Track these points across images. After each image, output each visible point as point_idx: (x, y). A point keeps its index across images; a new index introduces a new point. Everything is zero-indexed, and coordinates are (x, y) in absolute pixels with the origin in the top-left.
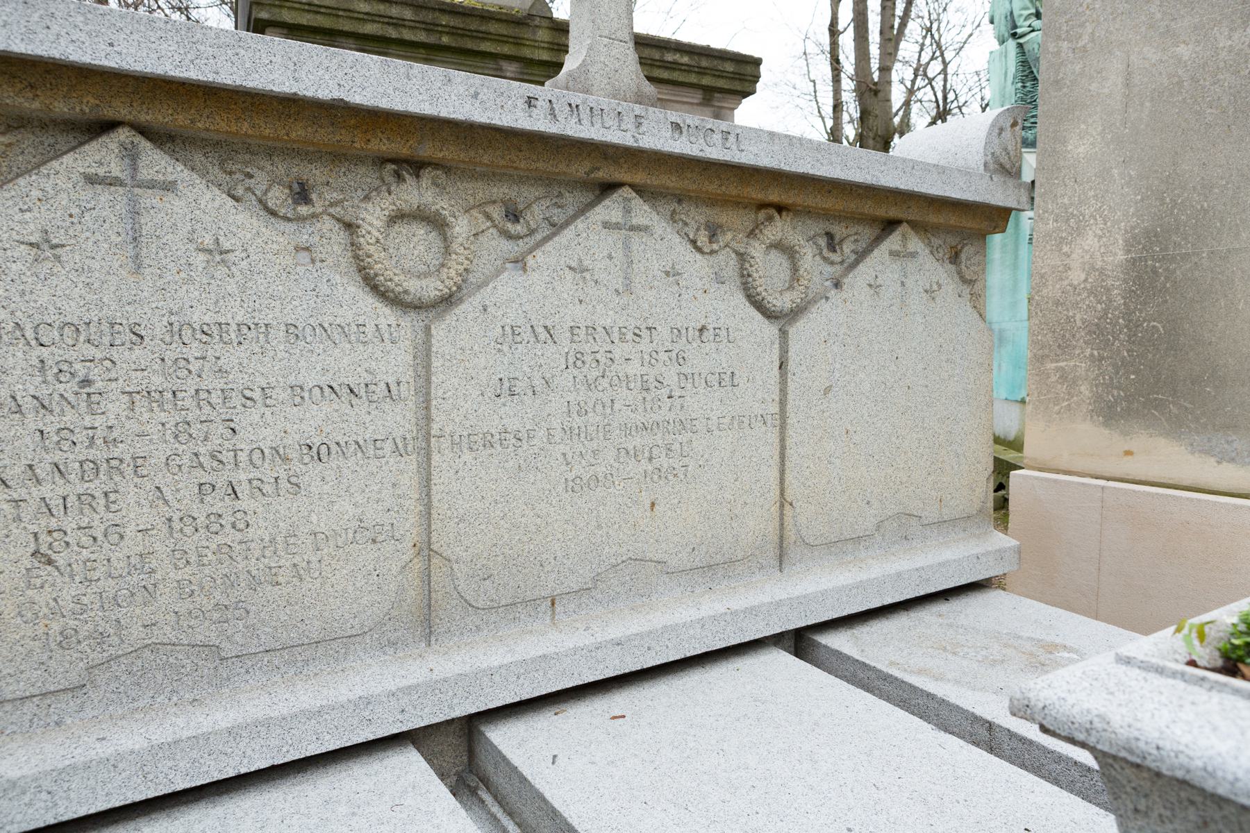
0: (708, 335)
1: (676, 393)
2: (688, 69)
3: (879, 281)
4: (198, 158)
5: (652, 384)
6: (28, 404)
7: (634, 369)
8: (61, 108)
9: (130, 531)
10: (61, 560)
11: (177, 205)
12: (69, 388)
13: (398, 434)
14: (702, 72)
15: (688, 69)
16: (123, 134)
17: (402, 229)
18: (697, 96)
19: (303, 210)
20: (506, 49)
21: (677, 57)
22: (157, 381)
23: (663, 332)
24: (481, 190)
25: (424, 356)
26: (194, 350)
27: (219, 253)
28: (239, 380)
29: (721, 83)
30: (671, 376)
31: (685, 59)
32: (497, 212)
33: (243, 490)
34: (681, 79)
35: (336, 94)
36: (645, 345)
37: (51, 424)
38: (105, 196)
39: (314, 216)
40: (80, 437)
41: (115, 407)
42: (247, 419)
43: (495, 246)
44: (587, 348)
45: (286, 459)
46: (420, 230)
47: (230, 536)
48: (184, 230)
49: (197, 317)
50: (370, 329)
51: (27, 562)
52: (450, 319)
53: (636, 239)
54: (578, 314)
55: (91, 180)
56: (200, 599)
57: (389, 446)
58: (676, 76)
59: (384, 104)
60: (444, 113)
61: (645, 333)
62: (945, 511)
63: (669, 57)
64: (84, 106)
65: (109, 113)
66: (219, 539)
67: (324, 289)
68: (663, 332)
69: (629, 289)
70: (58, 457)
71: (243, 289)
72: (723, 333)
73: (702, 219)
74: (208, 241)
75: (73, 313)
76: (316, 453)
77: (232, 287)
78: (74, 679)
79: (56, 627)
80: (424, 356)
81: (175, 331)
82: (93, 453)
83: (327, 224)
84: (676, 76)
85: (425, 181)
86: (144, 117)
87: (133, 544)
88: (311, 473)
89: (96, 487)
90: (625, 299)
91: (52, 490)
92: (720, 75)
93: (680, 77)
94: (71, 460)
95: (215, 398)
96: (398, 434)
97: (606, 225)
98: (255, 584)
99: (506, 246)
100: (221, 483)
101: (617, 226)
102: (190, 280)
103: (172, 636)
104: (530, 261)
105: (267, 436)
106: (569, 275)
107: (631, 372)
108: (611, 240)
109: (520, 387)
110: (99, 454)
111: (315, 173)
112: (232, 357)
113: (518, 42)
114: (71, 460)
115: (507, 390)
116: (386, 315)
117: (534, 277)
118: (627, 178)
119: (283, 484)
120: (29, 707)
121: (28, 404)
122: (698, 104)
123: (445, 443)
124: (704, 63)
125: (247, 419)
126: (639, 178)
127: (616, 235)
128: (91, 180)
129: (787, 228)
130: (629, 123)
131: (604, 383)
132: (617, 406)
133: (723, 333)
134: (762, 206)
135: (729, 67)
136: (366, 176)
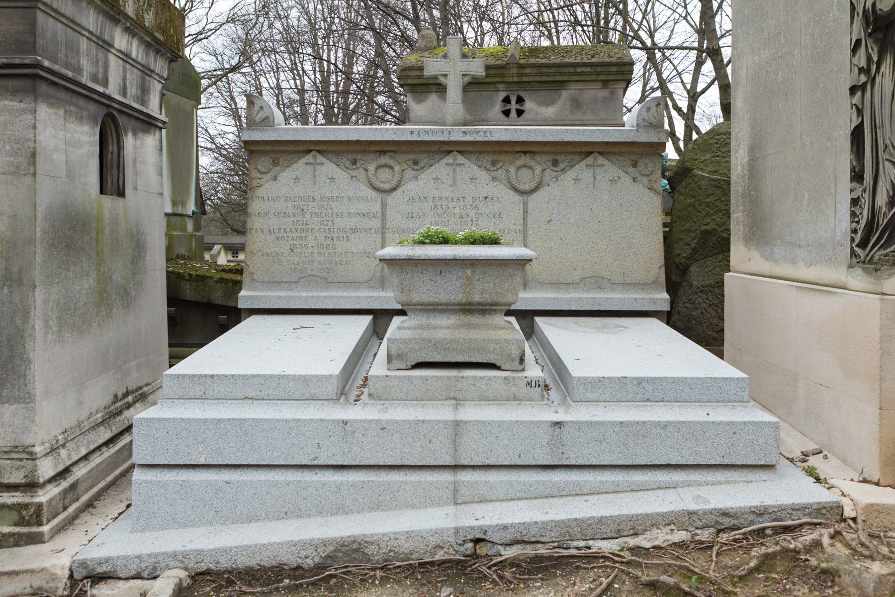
0: (489, 199)
1: (474, 220)
2: (591, 74)
3: (579, 177)
4: (330, 156)
5: (464, 216)
6: (291, 214)
7: (457, 211)
8: (301, 149)
9: (309, 246)
10: (295, 251)
11: (324, 168)
12: (299, 211)
13: (376, 227)
14: (599, 74)
15: (591, 74)
16: (313, 153)
17: (381, 170)
18: (599, 85)
19: (354, 167)
20: (497, 79)
21: (584, 69)
22: (317, 210)
23: (469, 198)
24: (407, 157)
25: (384, 205)
26: (326, 203)
27: (332, 179)
28: (336, 211)
29: (610, 77)
30: (472, 214)
31: (588, 69)
32: (410, 163)
33: (335, 239)
34: (586, 79)
35: (357, 139)
36: (461, 203)
37: (295, 219)
38: (309, 167)
39: (358, 168)
40: (301, 223)
41: (308, 216)
42: (337, 221)
43: (410, 173)
44: (439, 204)
45: (346, 232)
46: (387, 170)
47: (331, 251)
48: (325, 174)
49: (327, 195)
50: (369, 198)
51: (289, 250)
52: (393, 195)
53: (458, 169)
54: (436, 193)
55: (307, 164)
56: (324, 265)
57: (373, 231)
58: (584, 78)
59: (369, 139)
60: (386, 139)
61: (462, 199)
62: (626, 279)
63: (579, 70)
64: (305, 148)
65: (310, 148)
66: (329, 251)
67: (358, 187)
68: (469, 198)
69: (454, 184)
70: (296, 227)
71: (338, 188)
72: (496, 199)
73: (490, 159)
74: (330, 176)
75: (301, 194)
76: (353, 231)
77: (335, 188)
78: (296, 280)
79: (293, 267)
80: (384, 205)
81: (322, 198)
82: (303, 227)
83: (361, 170)
84: (584, 78)
85: (387, 156)
86: (317, 149)
87: (310, 250)
88: (352, 236)
89: (303, 235)
90: (454, 188)
91: (294, 235)
92: (609, 74)
93: (586, 78)
94: (299, 228)
95: (330, 215)
96: (376, 227)
97: (447, 164)
98: (336, 264)
99: (414, 173)
100: (330, 236)
101: (451, 164)
102: (325, 186)
103: (317, 274)
104: (419, 177)
105: (342, 226)
106: (433, 181)
107: (456, 212)
108: (449, 169)
109: (414, 215)
110: (304, 227)
111: (358, 157)
112: (334, 205)
113: (502, 76)
114: (299, 228)
115: (410, 216)
116: (374, 194)
117: (421, 182)
118: (453, 149)
119: (345, 238)
120: (287, 284)
121: (291, 214)
122: (601, 88)
123: (390, 231)
124: (599, 69)
125: (337, 221)
126: (458, 148)
127: (450, 167)
128: (307, 164)
129: (527, 160)
130: (446, 134)
131: (445, 215)
132: (450, 223)
133: (496, 199)
134: (518, 152)
135: (614, 69)
136: (372, 156)
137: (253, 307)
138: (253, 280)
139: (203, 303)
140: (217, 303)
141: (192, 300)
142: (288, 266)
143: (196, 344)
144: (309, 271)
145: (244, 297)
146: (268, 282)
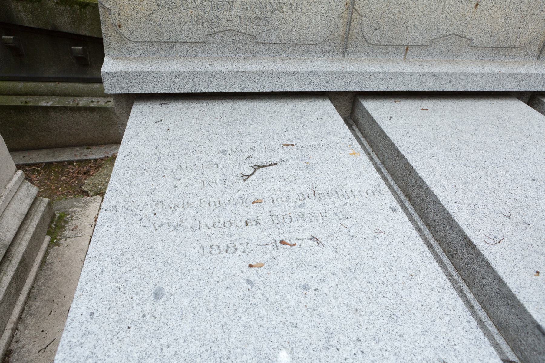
78: (201, 38)
79: (195, 14)
98: (273, 10)
103: (238, 28)
120: (186, 46)
137: (132, 91)
138: (122, 37)
139: (48, 30)
140: (66, 31)
141: (32, 26)
142: (184, 13)
143: (52, 78)
144: (224, 23)
145: (113, 74)
146: (151, 43)
